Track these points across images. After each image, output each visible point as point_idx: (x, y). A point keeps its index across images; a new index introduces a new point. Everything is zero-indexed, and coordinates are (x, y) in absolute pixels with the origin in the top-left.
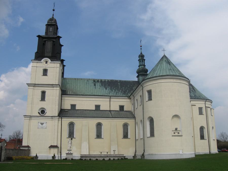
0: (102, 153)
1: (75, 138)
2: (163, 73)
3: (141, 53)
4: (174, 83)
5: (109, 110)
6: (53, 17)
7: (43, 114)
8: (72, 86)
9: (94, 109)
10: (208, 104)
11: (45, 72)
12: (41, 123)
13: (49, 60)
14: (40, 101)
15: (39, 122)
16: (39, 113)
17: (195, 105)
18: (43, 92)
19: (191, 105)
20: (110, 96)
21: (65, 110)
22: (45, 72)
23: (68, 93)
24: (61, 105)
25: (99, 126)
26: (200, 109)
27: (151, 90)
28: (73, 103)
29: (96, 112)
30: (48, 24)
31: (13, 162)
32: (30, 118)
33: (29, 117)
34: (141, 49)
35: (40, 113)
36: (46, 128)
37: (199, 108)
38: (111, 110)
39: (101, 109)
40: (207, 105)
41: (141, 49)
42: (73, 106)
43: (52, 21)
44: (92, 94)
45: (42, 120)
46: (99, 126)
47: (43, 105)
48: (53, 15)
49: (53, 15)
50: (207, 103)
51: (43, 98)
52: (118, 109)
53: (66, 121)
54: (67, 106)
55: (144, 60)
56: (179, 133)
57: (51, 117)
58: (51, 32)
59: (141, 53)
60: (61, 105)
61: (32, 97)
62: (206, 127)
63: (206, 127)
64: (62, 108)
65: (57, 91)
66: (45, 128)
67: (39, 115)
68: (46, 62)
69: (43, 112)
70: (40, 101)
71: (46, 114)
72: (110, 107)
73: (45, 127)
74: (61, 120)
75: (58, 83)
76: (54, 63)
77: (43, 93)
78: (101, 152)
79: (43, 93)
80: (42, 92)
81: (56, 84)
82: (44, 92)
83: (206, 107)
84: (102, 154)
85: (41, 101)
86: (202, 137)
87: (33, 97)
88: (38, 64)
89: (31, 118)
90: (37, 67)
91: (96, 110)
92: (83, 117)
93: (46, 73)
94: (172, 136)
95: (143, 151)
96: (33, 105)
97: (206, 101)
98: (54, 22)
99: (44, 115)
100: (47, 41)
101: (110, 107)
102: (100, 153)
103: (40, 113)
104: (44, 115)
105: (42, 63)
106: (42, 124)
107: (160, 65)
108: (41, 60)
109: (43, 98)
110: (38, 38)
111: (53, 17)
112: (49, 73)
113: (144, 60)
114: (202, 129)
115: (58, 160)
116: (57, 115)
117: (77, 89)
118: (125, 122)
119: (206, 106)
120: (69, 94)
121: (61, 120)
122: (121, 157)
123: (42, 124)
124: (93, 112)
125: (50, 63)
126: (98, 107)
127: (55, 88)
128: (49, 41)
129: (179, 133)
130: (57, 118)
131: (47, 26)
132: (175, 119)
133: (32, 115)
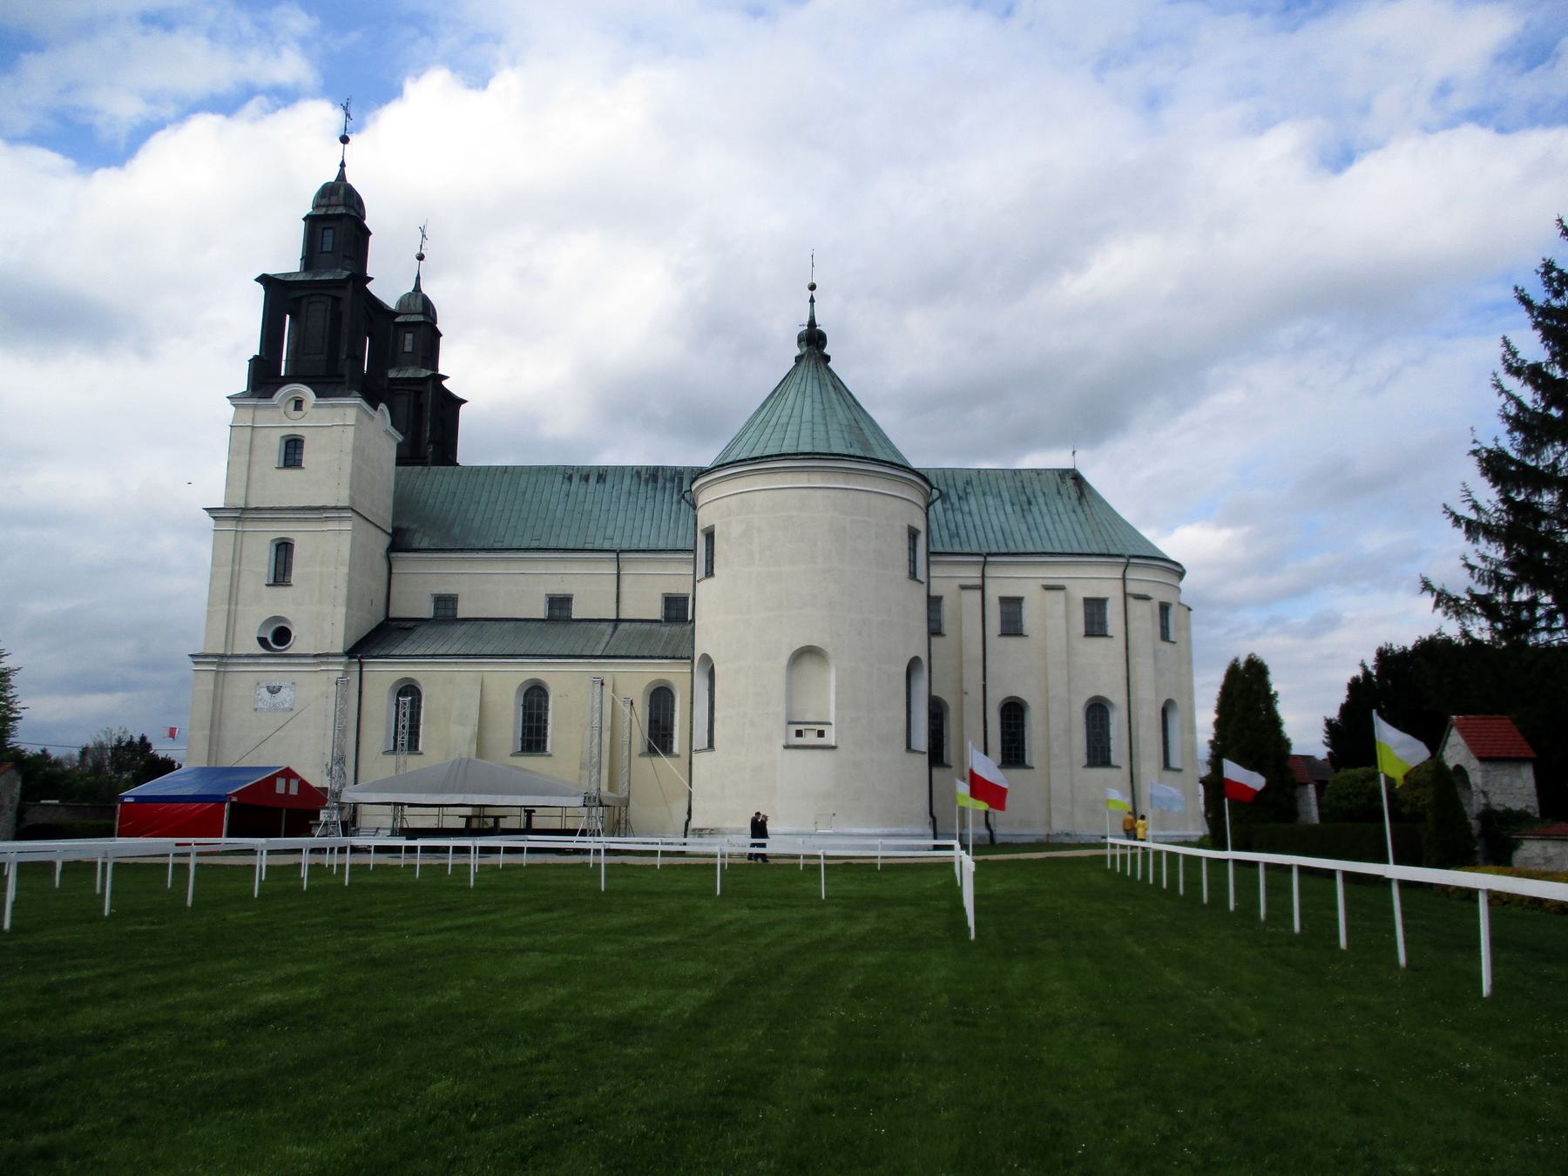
2: (798, 446)
3: (812, 323)
4: (728, 498)
6: (341, 176)
7: (283, 645)
8: (455, 505)
10: (1141, 580)
11: (292, 452)
12: (268, 688)
13: (307, 393)
15: (258, 684)
16: (263, 641)
17: (1061, 588)
19: (1043, 586)
20: (619, 552)
21: (403, 624)
22: (292, 452)
23: (416, 546)
25: (535, 700)
26: (1095, 611)
27: (714, 526)
28: (558, 589)
29: (666, 630)
30: (322, 211)
32: (219, 664)
33: (216, 660)
34: (812, 300)
35: (270, 639)
37: (1087, 601)
38: (622, 616)
39: (577, 612)
40: (1133, 588)
41: (812, 300)
42: (445, 604)
43: (334, 200)
44: (535, 544)
45: (274, 671)
46: (535, 700)
47: (282, 604)
48: (343, 165)
49: (343, 165)
50: (1132, 574)
51: (281, 574)
52: (656, 611)
53: (383, 675)
54: (415, 601)
56: (821, 734)
57: (316, 656)
58: (329, 252)
59: (812, 323)
61: (230, 569)
63: (1117, 698)
67: (264, 651)
68: (298, 404)
71: (290, 649)
72: (618, 602)
73: (287, 705)
74: (361, 672)
75: (352, 498)
76: (333, 406)
77: (284, 549)
79: (284, 549)
81: (340, 504)
82: (287, 544)
83: (1125, 594)
86: (1098, 755)
87: (237, 568)
88: (260, 414)
89: (226, 664)
90: (253, 427)
91: (551, 619)
92: (459, 656)
93: (297, 457)
94: (787, 747)
95: (687, 817)
96: (236, 604)
97: (1127, 565)
98: (342, 201)
99: (283, 650)
100: (305, 302)
101: (618, 602)
103: (270, 639)
104: (283, 650)
105: (276, 406)
106: (273, 691)
108: (270, 396)
109: (281, 574)
110: (260, 290)
111: (341, 176)
112: (308, 456)
114: (1097, 711)
117: (473, 520)
118: (656, 677)
119: (1128, 591)
121: (361, 672)
123: (273, 691)
124: (580, 626)
125: (316, 406)
126: (559, 605)
128: (314, 299)
129: (797, 731)
130: (341, 663)
131: (308, 221)
132: (809, 666)
133: (229, 653)
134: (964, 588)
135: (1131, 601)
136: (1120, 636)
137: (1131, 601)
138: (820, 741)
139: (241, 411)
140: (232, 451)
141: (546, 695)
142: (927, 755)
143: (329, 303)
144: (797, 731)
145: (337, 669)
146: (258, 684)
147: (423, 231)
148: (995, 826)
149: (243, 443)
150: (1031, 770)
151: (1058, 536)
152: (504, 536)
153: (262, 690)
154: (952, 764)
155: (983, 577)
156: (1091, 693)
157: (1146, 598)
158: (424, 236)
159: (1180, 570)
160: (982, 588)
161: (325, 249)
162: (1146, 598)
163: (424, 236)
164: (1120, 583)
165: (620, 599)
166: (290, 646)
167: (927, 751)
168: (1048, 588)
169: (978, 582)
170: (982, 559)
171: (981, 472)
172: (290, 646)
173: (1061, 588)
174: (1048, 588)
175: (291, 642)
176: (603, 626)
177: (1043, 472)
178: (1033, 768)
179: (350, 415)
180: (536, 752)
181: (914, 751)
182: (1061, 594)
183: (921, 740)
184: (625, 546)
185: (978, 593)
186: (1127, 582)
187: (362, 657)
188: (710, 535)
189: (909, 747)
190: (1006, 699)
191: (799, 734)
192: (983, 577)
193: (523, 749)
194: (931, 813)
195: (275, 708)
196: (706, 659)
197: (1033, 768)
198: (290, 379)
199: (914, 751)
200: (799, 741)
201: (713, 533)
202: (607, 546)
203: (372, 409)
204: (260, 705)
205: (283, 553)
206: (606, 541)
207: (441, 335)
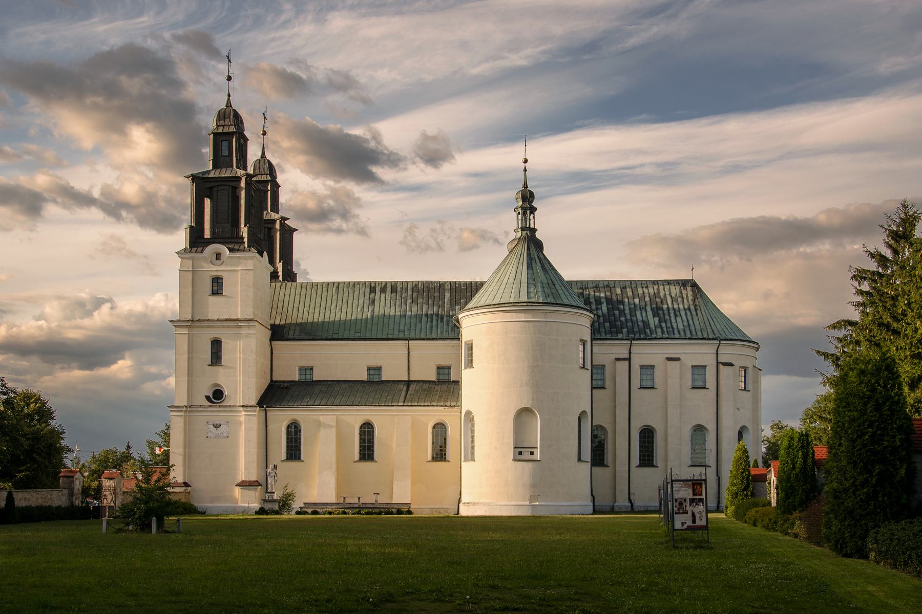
0: (346, 498)
1: (303, 461)
5: (407, 379)
6: (229, 104)
9: (364, 377)
10: (728, 352)
14: (209, 365)
16: (208, 398)
17: (678, 359)
18: (214, 341)
22: (217, 286)
23: (291, 336)
24: (272, 370)
27: (472, 340)
31: (776, 508)
35: (211, 397)
36: (228, 437)
38: (411, 379)
44: (357, 335)
46: (367, 430)
51: (216, 358)
53: (281, 417)
54: (289, 373)
55: (535, 209)
56: (532, 453)
58: (226, 156)
60: (272, 370)
62: (711, 427)
64: (274, 379)
65: (258, 337)
66: (224, 437)
68: (218, 256)
69: (218, 395)
70: (209, 365)
72: (409, 370)
73: (225, 435)
77: (216, 345)
78: (359, 496)
80: (212, 342)
83: (718, 363)
84: (346, 502)
85: (210, 367)
100: (215, 189)
101: (409, 370)
102: (343, 498)
103: (211, 397)
106: (217, 426)
107: (505, 266)
113: (535, 209)
115: (345, 508)
116: (254, 403)
120: (292, 337)
122: (368, 509)
123: (217, 426)
127: (244, 331)
128: (220, 188)
129: (519, 452)
134: (618, 359)
135: (721, 366)
136: (713, 389)
137: (721, 366)
138: (532, 457)
139: (185, 261)
140: (182, 286)
141: (373, 428)
142: (590, 463)
143: (230, 190)
144: (519, 452)
145: (257, 412)
146: (208, 422)
147: (264, 115)
148: (634, 501)
149: (189, 280)
150: (656, 468)
151: (677, 325)
152: (339, 330)
153: (210, 426)
154: (609, 465)
155: (630, 353)
156: (695, 423)
157: (731, 365)
158: (265, 118)
159: (756, 346)
160: (629, 359)
161: (224, 154)
162: (731, 365)
163: (265, 118)
164: (715, 356)
165: (410, 369)
166: (224, 400)
167: (590, 461)
168: (669, 359)
169: (627, 356)
170: (629, 342)
171: (633, 283)
172: (224, 400)
173: (678, 359)
174: (669, 359)
175: (224, 398)
176: (401, 386)
177: (672, 282)
178: (658, 467)
179: (250, 264)
180: (368, 460)
181: (582, 461)
182: (678, 363)
183: (587, 454)
184: (412, 336)
185: (627, 362)
186: (719, 355)
187: (267, 407)
188: (470, 348)
189: (579, 460)
190: (643, 426)
191: (520, 453)
192: (630, 353)
193: (360, 459)
194: (592, 495)
195: (218, 436)
196: (469, 413)
197: (658, 467)
198: (214, 239)
199: (582, 461)
200: (521, 457)
201: (472, 347)
202: (401, 336)
203: (260, 257)
204: (209, 434)
205: (216, 346)
206: (400, 333)
207: (280, 186)
